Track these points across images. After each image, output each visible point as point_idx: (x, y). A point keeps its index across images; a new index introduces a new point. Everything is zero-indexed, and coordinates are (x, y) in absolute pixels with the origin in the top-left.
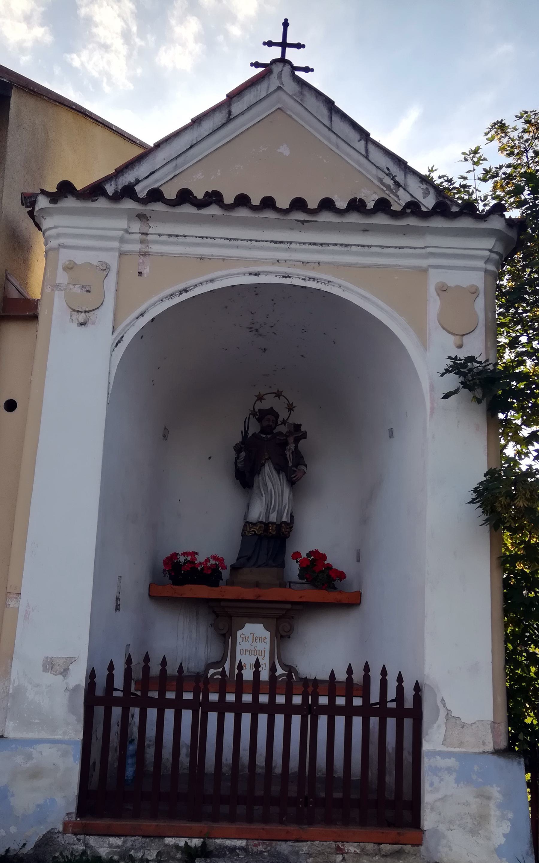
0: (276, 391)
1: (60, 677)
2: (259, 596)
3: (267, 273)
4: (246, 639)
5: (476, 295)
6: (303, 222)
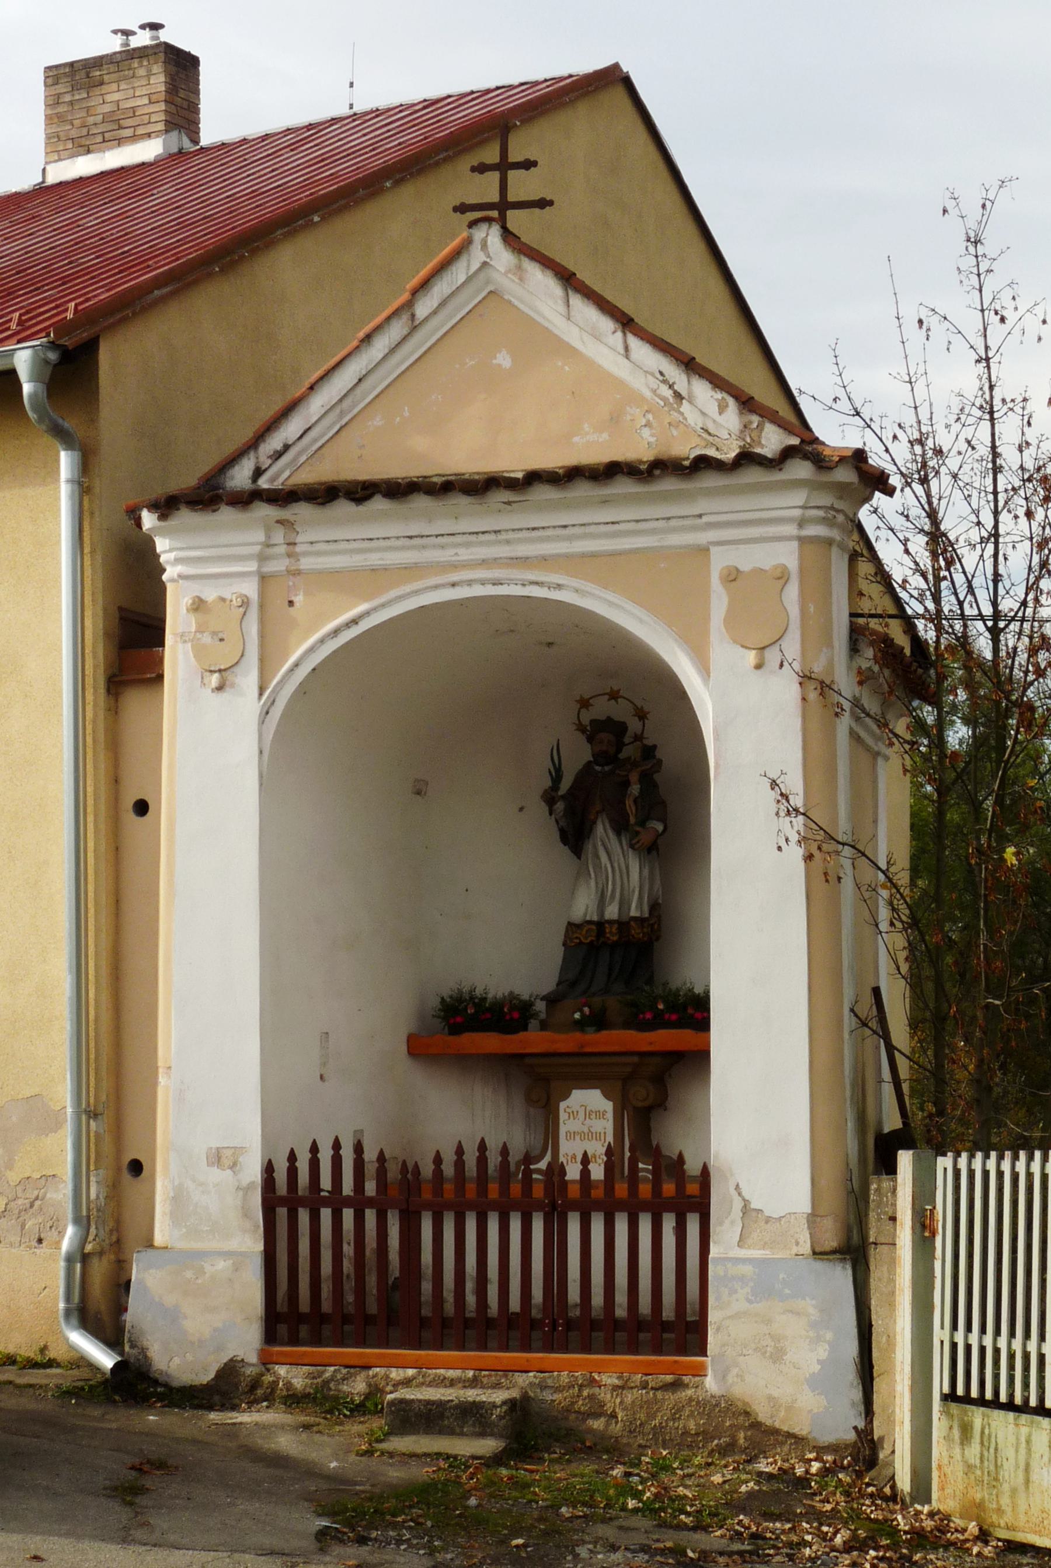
0: (608, 691)
1: (229, 1172)
2: (582, 1047)
3: (470, 583)
4: (573, 1115)
5: (782, 581)
6: (509, 503)
